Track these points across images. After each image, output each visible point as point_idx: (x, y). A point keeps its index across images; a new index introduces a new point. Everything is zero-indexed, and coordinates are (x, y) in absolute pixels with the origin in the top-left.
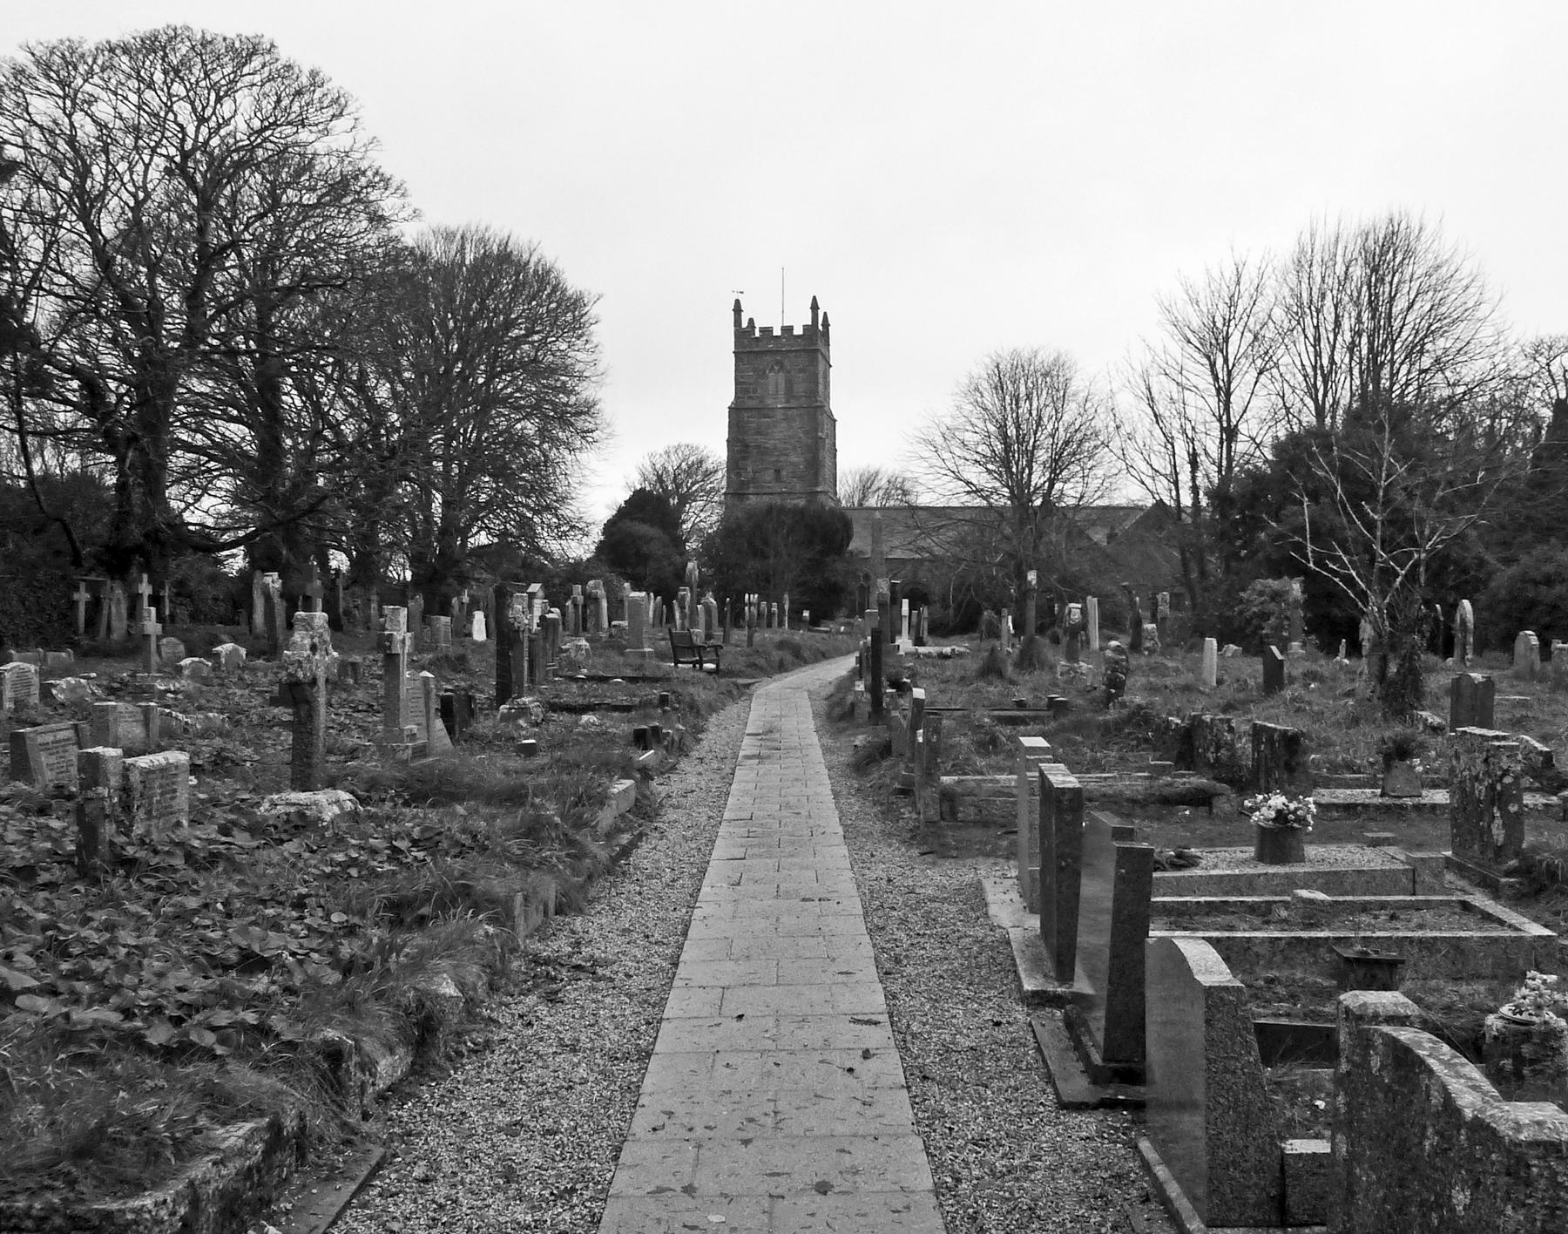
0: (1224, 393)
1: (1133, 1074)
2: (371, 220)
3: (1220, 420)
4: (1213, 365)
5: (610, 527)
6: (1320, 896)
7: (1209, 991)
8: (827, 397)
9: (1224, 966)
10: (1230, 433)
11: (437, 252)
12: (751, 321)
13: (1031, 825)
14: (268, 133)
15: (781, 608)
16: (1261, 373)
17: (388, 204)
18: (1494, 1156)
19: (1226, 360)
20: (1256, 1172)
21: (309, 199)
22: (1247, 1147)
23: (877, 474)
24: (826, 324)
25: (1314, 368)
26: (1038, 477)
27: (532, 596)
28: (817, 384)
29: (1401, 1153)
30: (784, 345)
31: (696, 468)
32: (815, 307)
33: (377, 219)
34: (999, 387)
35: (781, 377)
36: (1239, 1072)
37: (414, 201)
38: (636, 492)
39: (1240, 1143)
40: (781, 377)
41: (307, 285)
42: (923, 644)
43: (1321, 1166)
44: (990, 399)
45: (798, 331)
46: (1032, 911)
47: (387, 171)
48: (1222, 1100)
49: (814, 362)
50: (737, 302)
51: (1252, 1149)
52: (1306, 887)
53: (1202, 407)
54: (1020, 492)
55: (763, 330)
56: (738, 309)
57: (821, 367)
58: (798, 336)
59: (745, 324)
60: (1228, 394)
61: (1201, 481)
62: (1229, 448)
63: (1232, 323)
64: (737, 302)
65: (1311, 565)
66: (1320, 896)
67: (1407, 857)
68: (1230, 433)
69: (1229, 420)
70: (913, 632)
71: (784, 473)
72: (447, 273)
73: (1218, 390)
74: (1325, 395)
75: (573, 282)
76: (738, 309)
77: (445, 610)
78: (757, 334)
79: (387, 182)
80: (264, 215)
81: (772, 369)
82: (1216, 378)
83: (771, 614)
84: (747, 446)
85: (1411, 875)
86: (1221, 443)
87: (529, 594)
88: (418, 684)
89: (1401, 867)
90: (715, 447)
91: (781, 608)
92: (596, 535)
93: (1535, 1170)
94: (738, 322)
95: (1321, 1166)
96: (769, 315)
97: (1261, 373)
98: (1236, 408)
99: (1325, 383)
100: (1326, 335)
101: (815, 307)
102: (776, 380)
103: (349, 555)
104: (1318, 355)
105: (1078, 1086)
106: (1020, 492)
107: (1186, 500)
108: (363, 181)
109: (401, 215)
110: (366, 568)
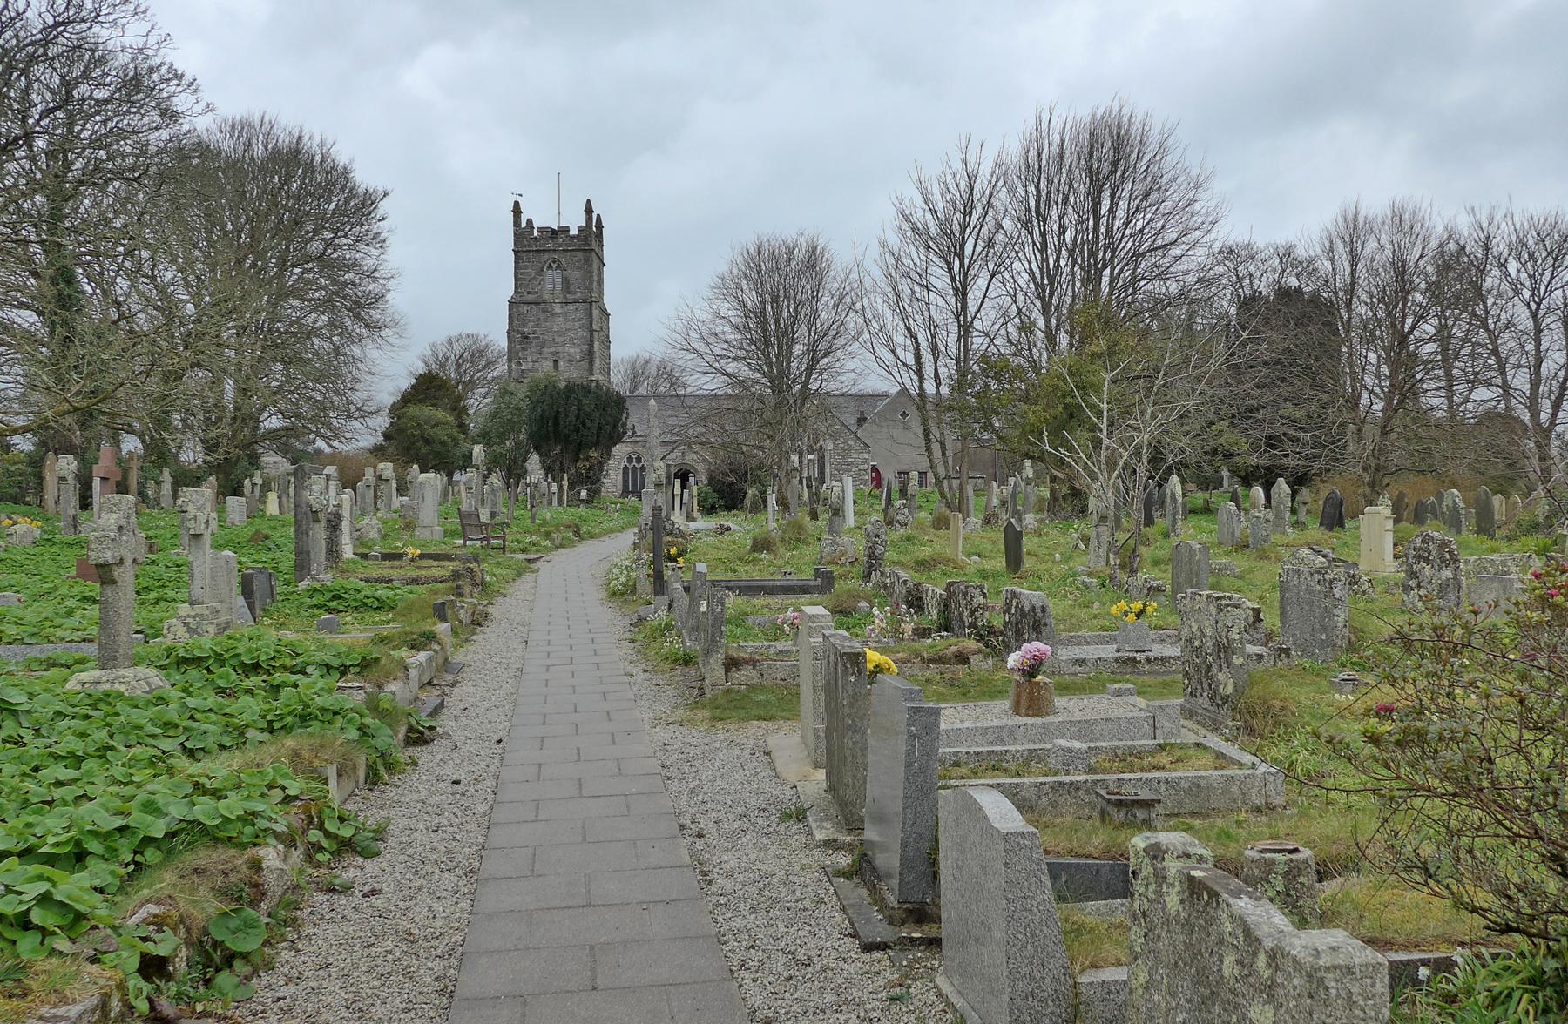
0: (961, 293)
1: (922, 913)
2: (162, 115)
3: (957, 318)
4: (950, 270)
5: (398, 409)
6: (1077, 745)
7: (1006, 837)
8: (601, 293)
9: (1017, 813)
10: (965, 329)
11: (226, 145)
12: (529, 222)
13: (815, 688)
14: (61, 28)
15: (560, 488)
16: (992, 276)
17: (180, 102)
18: (1295, 981)
19: (962, 264)
20: (1053, 1001)
21: (101, 94)
22: (1044, 978)
23: (647, 362)
24: (600, 226)
25: (1041, 270)
26: (797, 366)
27: (328, 477)
28: (591, 281)
29: (1201, 978)
30: (560, 245)
31: (476, 354)
32: (589, 210)
33: (170, 115)
34: (759, 284)
35: (558, 275)
36: (1036, 910)
37: (206, 96)
38: (420, 378)
39: (1038, 976)
40: (558, 275)
41: (96, 177)
42: (694, 520)
43: (1110, 992)
44: (751, 298)
45: (574, 232)
46: (817, 766)
47: (180, 66)
48: (1020, 936)
49: (588, 261)
50: (517, 204)
51: (1048, 981)
52: (1062, 736)
53: (942, 308)
54: (779, 380)
55: (541, 230)
56: (517, 211)
57: (596, 266)
58: (573, 237)
59: (524, 225)
60: (965, 295)
61: (943, 372)
62: (966, 345)
63: (968, 230)
64: (517, 204)
65: (1047, 448)
66: (1077, 745)
67: (1148, 705)
68: (965, 329)
69: (965, 319)
70: (684, 508)
71: (561, 363)
72: (235, 167)
73: (956, 289)
74: (1051, 295)
75: (365, 177)
76: (517, 211)
77: (237, 491)
78: (536, 234)
79: (179, 77)
80: (54, 110)
81: (550, 267)
82: (953, 279)
83: (551, 494)
84: (527, 338)
85: (1151, 722)
86: (959, 340)
87: (327, 475)
88: (222, 562)
89: (1143, 714)
90: (498, 337)
91: (560, 488)
92: (382, 422)
93: (1333, 992)
94: (517, 222)
95: (1110, 992)
96: (542, 216)
97: (992, 276)
98: (972, 308)
99: (1051, 283)
100: (1052, 242)
101: (589, 210)
102: (551, 280)
103: (143, 442)
104: (1045, 260)
105: (880, 930)
106: (779, 380)
107: (930, 387)
108: (155, 77)
109: (195, 110)
110: (158, 454)
